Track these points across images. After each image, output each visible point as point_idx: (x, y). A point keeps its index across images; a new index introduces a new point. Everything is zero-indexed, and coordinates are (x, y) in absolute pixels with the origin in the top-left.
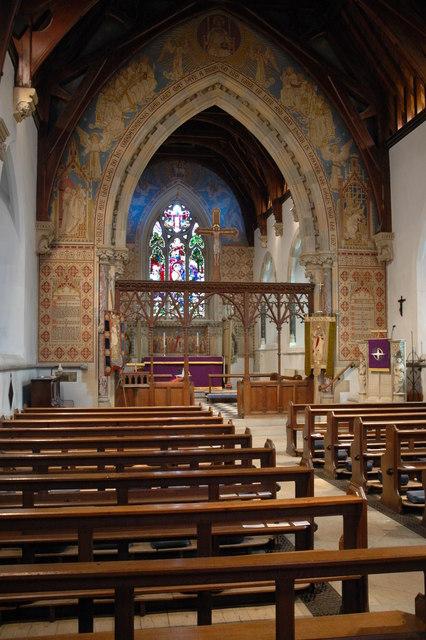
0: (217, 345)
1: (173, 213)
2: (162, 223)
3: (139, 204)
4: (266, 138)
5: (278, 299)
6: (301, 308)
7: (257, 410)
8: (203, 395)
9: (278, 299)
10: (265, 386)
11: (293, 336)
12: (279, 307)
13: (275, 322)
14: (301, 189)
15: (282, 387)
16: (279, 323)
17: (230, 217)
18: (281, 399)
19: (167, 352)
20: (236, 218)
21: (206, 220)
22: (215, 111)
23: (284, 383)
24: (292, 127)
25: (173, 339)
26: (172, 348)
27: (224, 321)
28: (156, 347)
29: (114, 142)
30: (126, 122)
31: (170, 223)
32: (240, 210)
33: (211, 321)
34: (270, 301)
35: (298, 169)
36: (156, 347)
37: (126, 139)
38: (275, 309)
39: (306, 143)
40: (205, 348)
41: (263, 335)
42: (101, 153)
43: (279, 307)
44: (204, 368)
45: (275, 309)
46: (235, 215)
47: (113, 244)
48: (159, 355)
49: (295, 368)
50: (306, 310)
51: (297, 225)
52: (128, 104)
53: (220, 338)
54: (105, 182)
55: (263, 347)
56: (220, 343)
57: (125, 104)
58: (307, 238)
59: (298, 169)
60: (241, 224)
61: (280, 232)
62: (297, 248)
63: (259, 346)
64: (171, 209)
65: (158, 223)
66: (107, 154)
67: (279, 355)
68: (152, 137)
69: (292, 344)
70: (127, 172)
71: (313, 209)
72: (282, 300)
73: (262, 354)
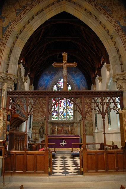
0: (78, 131)
1: (61, 82)
2: (57, 85)
3: (48, 78)
4: (90, 20)
5: (102, 100)
6: (116, 106)
7: (92, 169)
8: (70, 152)
9: (102, 100)
10: (97, 154)
11: (109, 125)
12: (103, 105)
13: (101, 114)
14: (110, 41)
15: (107, 154)
16: (103, 114)
17: (82, 82)
18: (107, 161)
19: (57, 134)
20: (84, 82)
21: (73, 83)
22: (65, 15)
23: (108, 152)
24: (103, 12)
25: (60, 128)
26: (60, 132)
27: (80, 121)
28: (53, 132)
29: (10, 23)
30: (17, 14)
31: (60, 85)
32: (85, 79)
33: (75, 121)
34: (97, 101)
35: (108, 32)
36: (53, 132)
37: (17, 21)
38: (100, 106)
39: (111, 19)
40: (73, 132)
41: (96, 126)
42: (3, 27)
43: (103, 105)
44: (72, 140)
45: (100, 106)
46: (83, 81)
47: (7, 72)
48: (54, 135)
49: (111, 140)
50: (119, 107)
51: (108, 73)
52: (19, 6)
53: (79, 128)
54: (4, 40)
55: (96, 131)
56: (79, 130)
57: (18, 7)
58: (116, 66)
59: (108, 32)
60: (86, 84)
61: (101, 81)
62: (109, 84)
63: (95, 131)
64: (60, 80)
65: (55, 85)
66: (6, 28)
67: (105, 134)
68: (31, 22)
69: (109, 129)
70: (17, 38)
71: (118, 51)
72: (104, 101)
73: (96, 134)
